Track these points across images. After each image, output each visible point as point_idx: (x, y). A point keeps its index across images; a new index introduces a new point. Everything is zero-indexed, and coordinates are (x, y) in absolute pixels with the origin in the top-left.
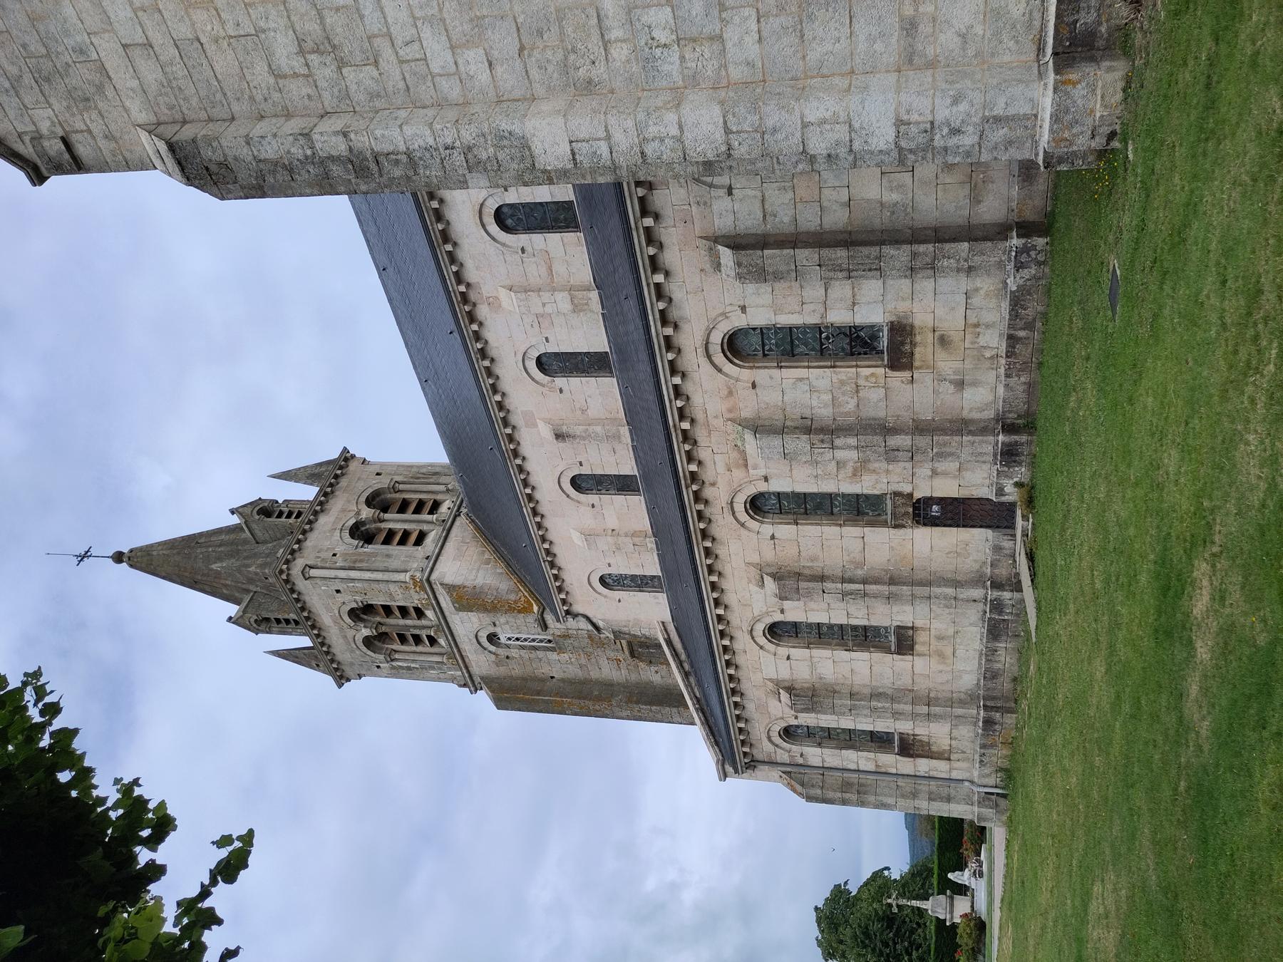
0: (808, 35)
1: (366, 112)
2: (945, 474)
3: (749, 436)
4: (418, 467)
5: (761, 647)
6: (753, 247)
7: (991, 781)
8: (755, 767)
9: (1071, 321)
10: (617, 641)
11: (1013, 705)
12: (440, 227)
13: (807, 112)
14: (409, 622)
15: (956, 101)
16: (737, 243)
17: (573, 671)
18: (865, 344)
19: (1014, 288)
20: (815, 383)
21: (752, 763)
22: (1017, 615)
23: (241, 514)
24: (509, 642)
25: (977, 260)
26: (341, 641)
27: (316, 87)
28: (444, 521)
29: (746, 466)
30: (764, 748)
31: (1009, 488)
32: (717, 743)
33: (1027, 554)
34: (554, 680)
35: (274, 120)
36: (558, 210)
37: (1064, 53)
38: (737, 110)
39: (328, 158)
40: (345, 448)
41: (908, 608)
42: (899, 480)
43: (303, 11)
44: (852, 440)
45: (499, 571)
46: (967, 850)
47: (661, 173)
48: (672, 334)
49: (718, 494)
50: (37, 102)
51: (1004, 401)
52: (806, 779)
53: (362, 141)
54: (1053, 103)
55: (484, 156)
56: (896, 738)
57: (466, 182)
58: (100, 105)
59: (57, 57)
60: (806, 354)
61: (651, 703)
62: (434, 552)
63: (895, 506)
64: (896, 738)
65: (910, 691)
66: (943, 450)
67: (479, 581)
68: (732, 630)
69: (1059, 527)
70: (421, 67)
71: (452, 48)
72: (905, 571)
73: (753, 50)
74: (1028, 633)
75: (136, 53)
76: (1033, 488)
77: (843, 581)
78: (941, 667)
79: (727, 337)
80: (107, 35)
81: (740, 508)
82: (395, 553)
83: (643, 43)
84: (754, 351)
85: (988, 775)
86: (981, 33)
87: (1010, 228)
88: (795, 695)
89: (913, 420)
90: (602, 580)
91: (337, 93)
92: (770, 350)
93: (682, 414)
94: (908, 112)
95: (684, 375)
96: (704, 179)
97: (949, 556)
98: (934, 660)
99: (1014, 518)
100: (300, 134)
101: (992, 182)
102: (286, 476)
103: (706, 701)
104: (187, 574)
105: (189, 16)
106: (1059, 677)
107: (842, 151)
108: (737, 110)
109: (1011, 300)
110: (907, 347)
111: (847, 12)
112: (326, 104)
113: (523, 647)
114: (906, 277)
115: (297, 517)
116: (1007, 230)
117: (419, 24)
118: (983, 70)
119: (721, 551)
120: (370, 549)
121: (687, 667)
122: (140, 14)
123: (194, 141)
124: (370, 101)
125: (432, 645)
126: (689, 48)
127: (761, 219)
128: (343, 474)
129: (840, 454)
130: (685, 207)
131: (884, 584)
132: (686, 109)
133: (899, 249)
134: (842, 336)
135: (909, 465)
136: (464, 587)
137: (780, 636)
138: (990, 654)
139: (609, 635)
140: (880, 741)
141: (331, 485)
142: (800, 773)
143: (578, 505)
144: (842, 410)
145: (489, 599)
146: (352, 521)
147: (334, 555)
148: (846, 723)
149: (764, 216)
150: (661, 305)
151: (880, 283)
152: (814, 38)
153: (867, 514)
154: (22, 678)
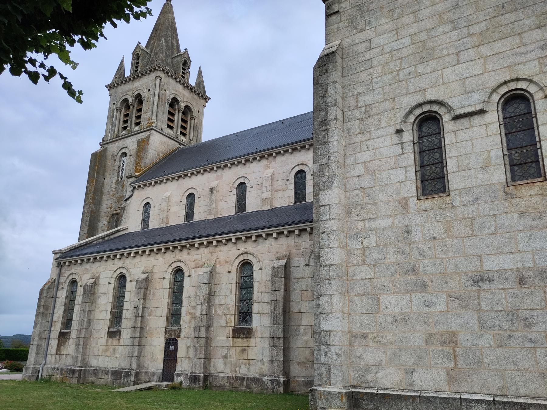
0: (364, 298)
1: (343, 127)
2: (188, 352)
3: (209, 269)
4: (201, 128)
5: (115, 272)
6: (285, 274)
7: (45, 373)
8: (58, 267)
9: (249, 402)
10: (120, 208)
11: (81, 382)
12: (299, 148)
13: (336, 296)
14: (134, 119)
15: (337, 354)
16: (287, 267)
17: (107, 188)
18: (244, 318)
19: (263, 379)
20: (229, 297)
21: (60, 266)
22: (123, 383)
23: (185, 53)
24: (122, 161)
25: (275, 364)
26: (127, 89)
27: (353, 110)
28: (177, 138)
29: (196, 268)
30: (67, 271)
31: (180, 379)
32: (71, 250)
33: (151, 387)
34: (103, 180)
35: (342, 92)
36: (303, 195)
37: (353, 396)
38: (338, 269)
39: (327, 111)
40: (210, 99)
41: (129, 336)
42: (186, 332)
43: (380, 108)
44: (204, 312)
45: (154, 160)
46: (7, 363)
47: (316, 239)
48: (252, 239)
49: (184, 255)
50: (352, 4)
51: (217, 376)
52: (51, 290)
53: (333, 125)
54: (334, 392)
55: (325, 171)
56: (68, 330)
57: (316, 163)
58: (350, 27)
59: (368, 14)
60: (241, 294)
61: (90, 221)
62: (164, 132)
63: (175, 330)
64: (68, 330)
65: (91, 336)
66: (198, 351)
67: (150, 151)
68: (124, 259)
69: (163, 400)
70: (358, 150)
71: (365, 162)
72: (146, 334)
73: (359, 276)
74: (115, 388)
75: (368, 44)
76: (180, 389)
77: (143, 308)
78: (101, 350)
79: (250, 262)
80: (375, 34)
81: (178, 264)
82: (165, 116)
83: (364, 234)
84: (244, 272)
85: (47, 371)
86: (361, 364)
87: (287, 377)
88: (92, 286)
89: (211, 338)
90: (148, 204)
91: (350, 117)
92: (244, 279)
93: (219, 242)
94: (334, 335)
95: (235, 243)
96: (313, 254)
97: (152, 354)
98: (104, 347)
99: (167, 381)
100: (336, 102)
101: (305, 370)
102: (200, 73)
103: (91, 246)
104: (160, 27)
105: (380, 65)
106: (97, 401)
107: (321, 310)
108: (338, 269)
109: (259, 378)
110: (242, 336)
111: (371, 313)
112: (347, 113)
113: (119, 167)
114: (270, 335)
115: (182, 76)
116: (287, 376)
117: (374, 151)
118: (348, 365)
119: (159, 256)
120: (167, 105)
121: (107, 238)
122: (382, 47)
123: (335, 61)
124: (347, 129)
125: (123, 128)
126: (361, 252)
127: (296, 277)
128: (199, 97)
129: (199, 307)
130: (302, 247)
131: (141, 325)
132: (339, 250)
133: (282, 332)
134: (248, 309)
135: (192, 336)
136: (148, 144)
137: (120, 280)
138: (106, 372)
139: (123, 205)
140: (67, 323)
141: (195, 92)
142: (54, 287)
143: (182, 195)
144: (217, 308)
145: (142, 154)
146: (179, 99)
147: (165, 90)
148: (77, 308)
149: (297, 278)
150: (264, 235)
151: (269, 325)
152: (362, 300)
153: (172, 318)
154: (150, 9)
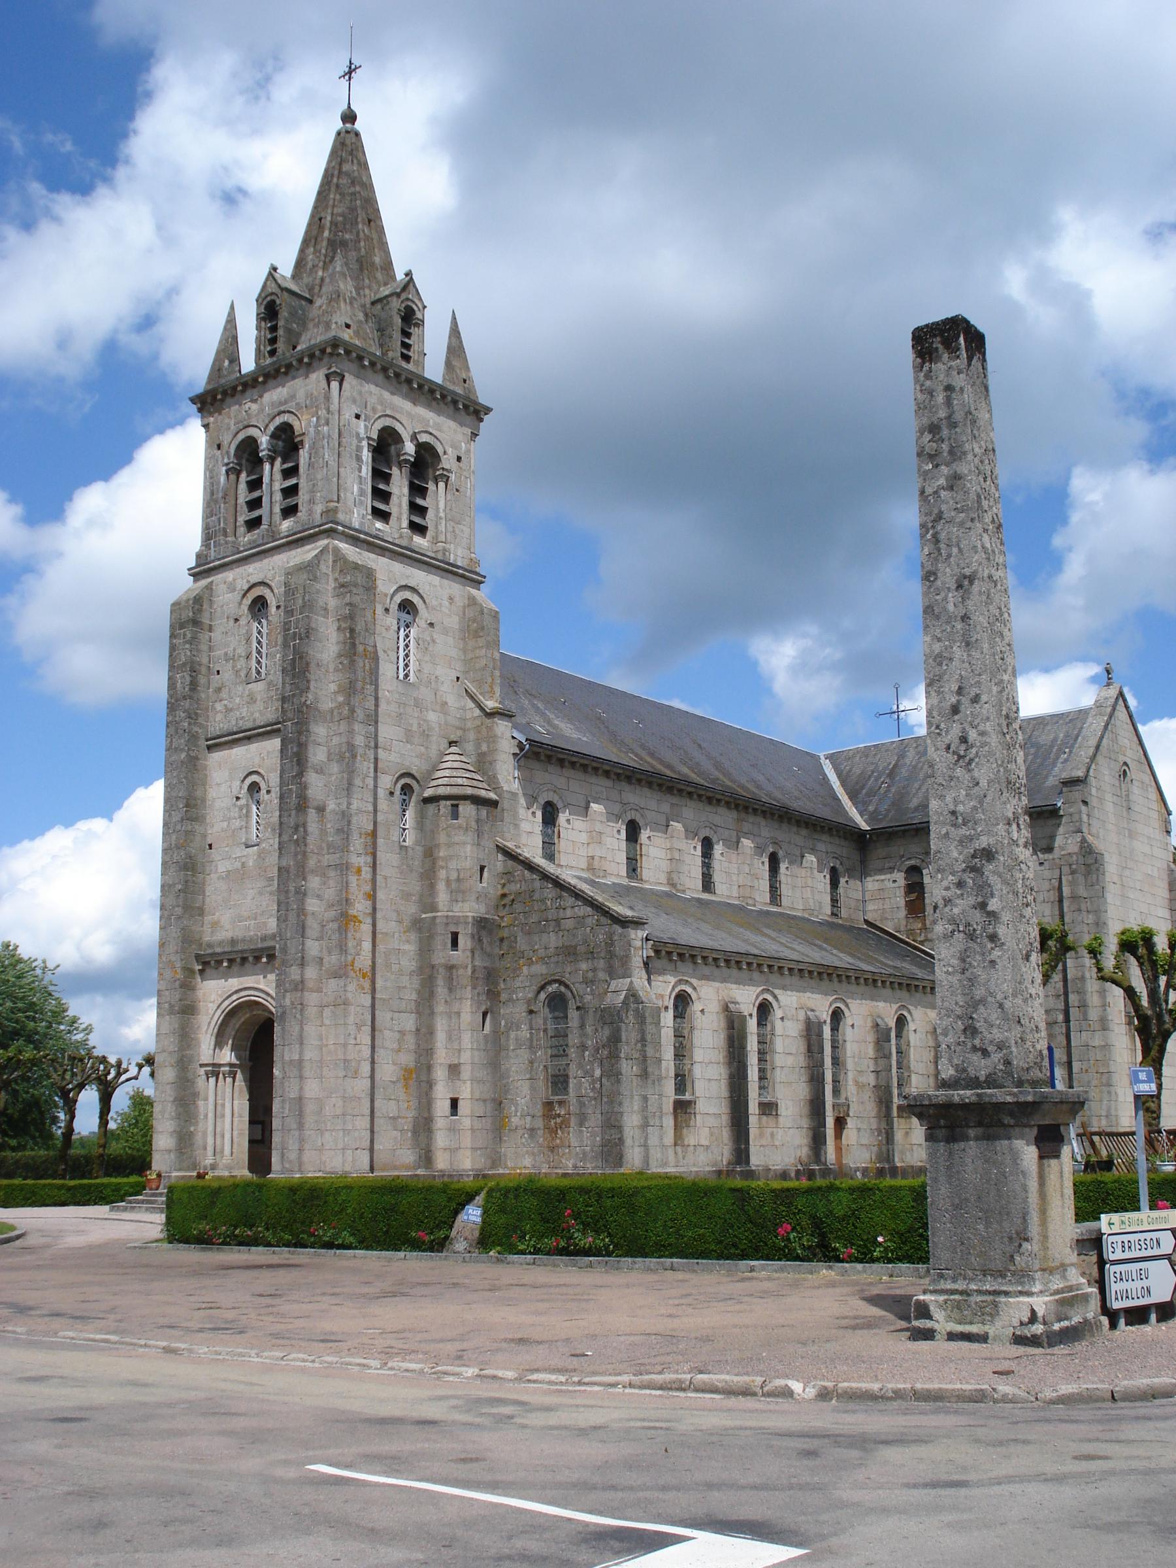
102: (455, 332)
